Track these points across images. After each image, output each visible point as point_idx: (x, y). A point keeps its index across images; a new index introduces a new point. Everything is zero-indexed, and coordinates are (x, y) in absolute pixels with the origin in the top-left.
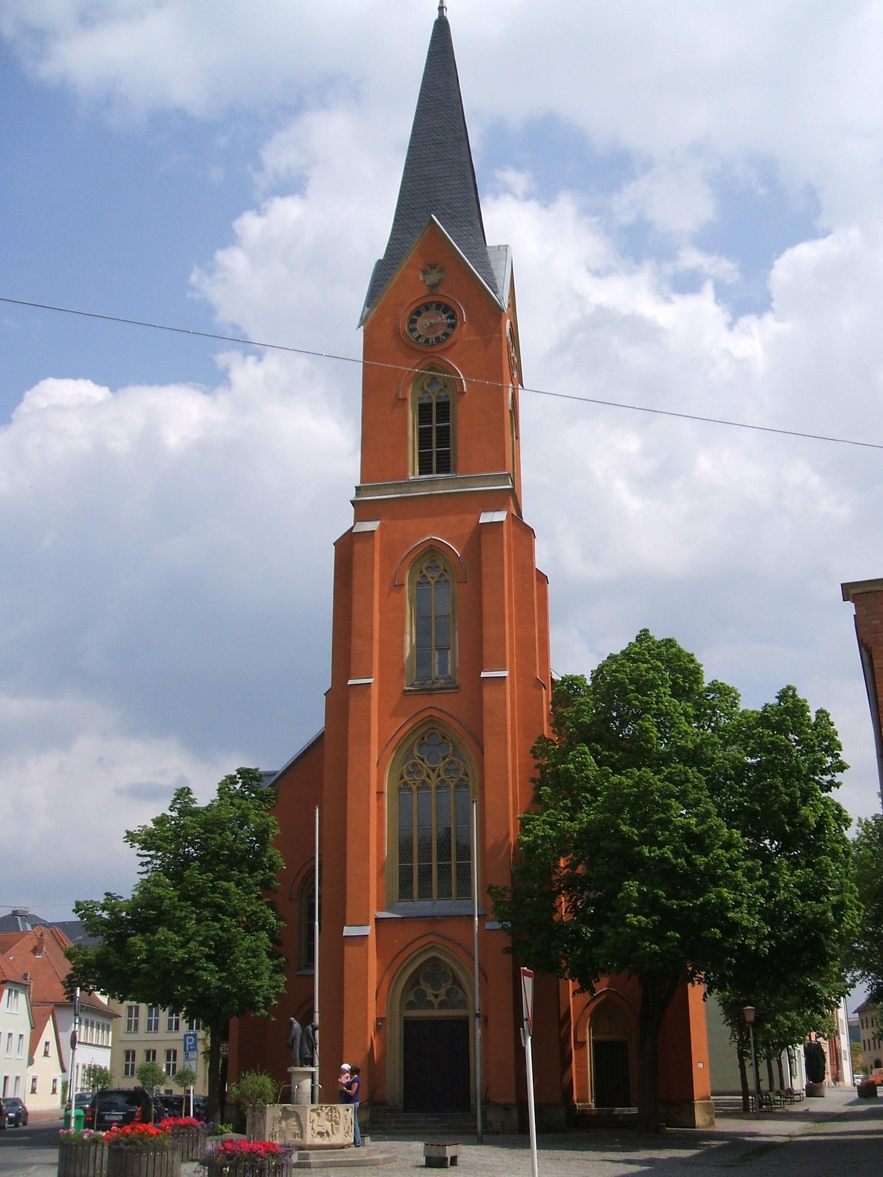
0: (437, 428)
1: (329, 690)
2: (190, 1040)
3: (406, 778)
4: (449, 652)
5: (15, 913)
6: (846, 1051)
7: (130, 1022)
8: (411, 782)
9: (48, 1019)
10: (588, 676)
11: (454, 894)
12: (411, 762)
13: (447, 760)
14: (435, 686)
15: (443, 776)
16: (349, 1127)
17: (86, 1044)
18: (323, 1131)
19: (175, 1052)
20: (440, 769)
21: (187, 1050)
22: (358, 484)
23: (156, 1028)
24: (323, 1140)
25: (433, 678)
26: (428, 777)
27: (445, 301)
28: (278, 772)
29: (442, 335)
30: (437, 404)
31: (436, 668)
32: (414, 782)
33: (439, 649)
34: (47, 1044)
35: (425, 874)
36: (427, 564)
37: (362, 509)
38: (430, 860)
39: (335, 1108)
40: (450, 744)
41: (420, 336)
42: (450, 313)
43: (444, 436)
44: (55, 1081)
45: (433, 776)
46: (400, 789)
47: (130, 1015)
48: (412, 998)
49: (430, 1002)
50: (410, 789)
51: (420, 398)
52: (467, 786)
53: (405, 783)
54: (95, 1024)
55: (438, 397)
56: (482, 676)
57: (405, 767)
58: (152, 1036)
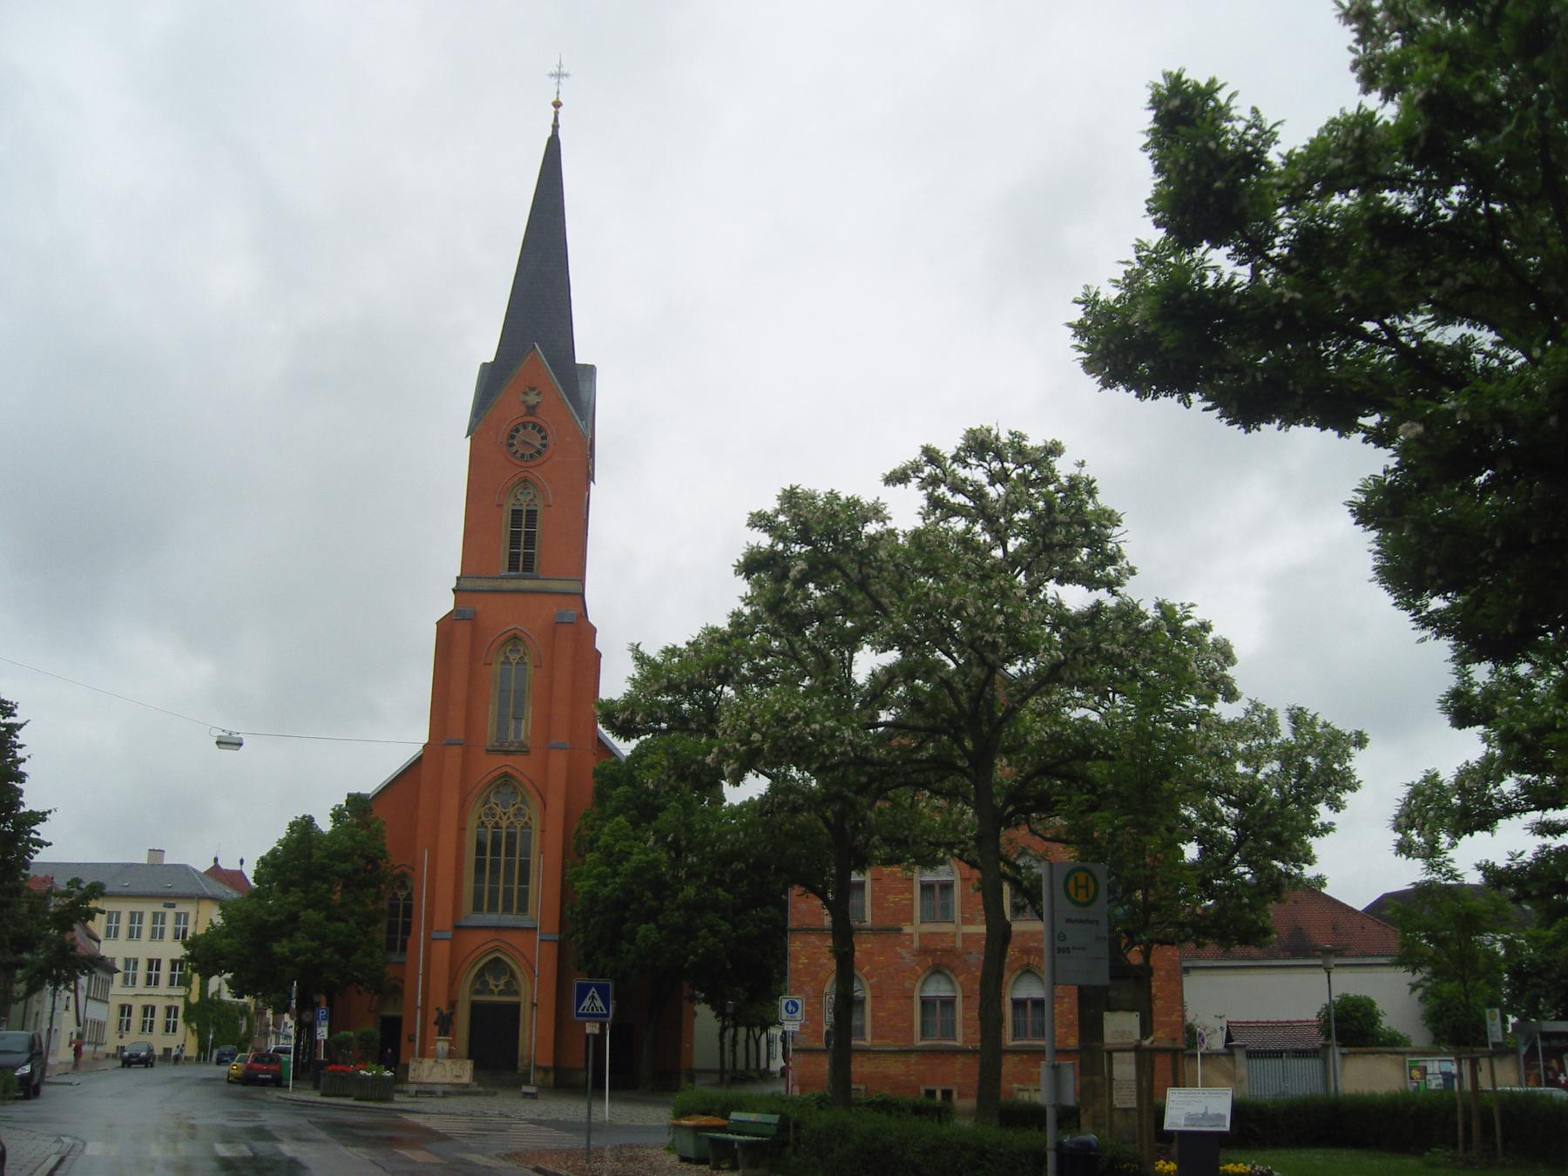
14: (512, 748)
19: (153, 1008)
27: (539, 422)
38: (504, 889)
42: (543, 434)
43: (530, 540)
45: (505, 818)
48: (478, 986)
52: (530, 828)
53: (483, 823)
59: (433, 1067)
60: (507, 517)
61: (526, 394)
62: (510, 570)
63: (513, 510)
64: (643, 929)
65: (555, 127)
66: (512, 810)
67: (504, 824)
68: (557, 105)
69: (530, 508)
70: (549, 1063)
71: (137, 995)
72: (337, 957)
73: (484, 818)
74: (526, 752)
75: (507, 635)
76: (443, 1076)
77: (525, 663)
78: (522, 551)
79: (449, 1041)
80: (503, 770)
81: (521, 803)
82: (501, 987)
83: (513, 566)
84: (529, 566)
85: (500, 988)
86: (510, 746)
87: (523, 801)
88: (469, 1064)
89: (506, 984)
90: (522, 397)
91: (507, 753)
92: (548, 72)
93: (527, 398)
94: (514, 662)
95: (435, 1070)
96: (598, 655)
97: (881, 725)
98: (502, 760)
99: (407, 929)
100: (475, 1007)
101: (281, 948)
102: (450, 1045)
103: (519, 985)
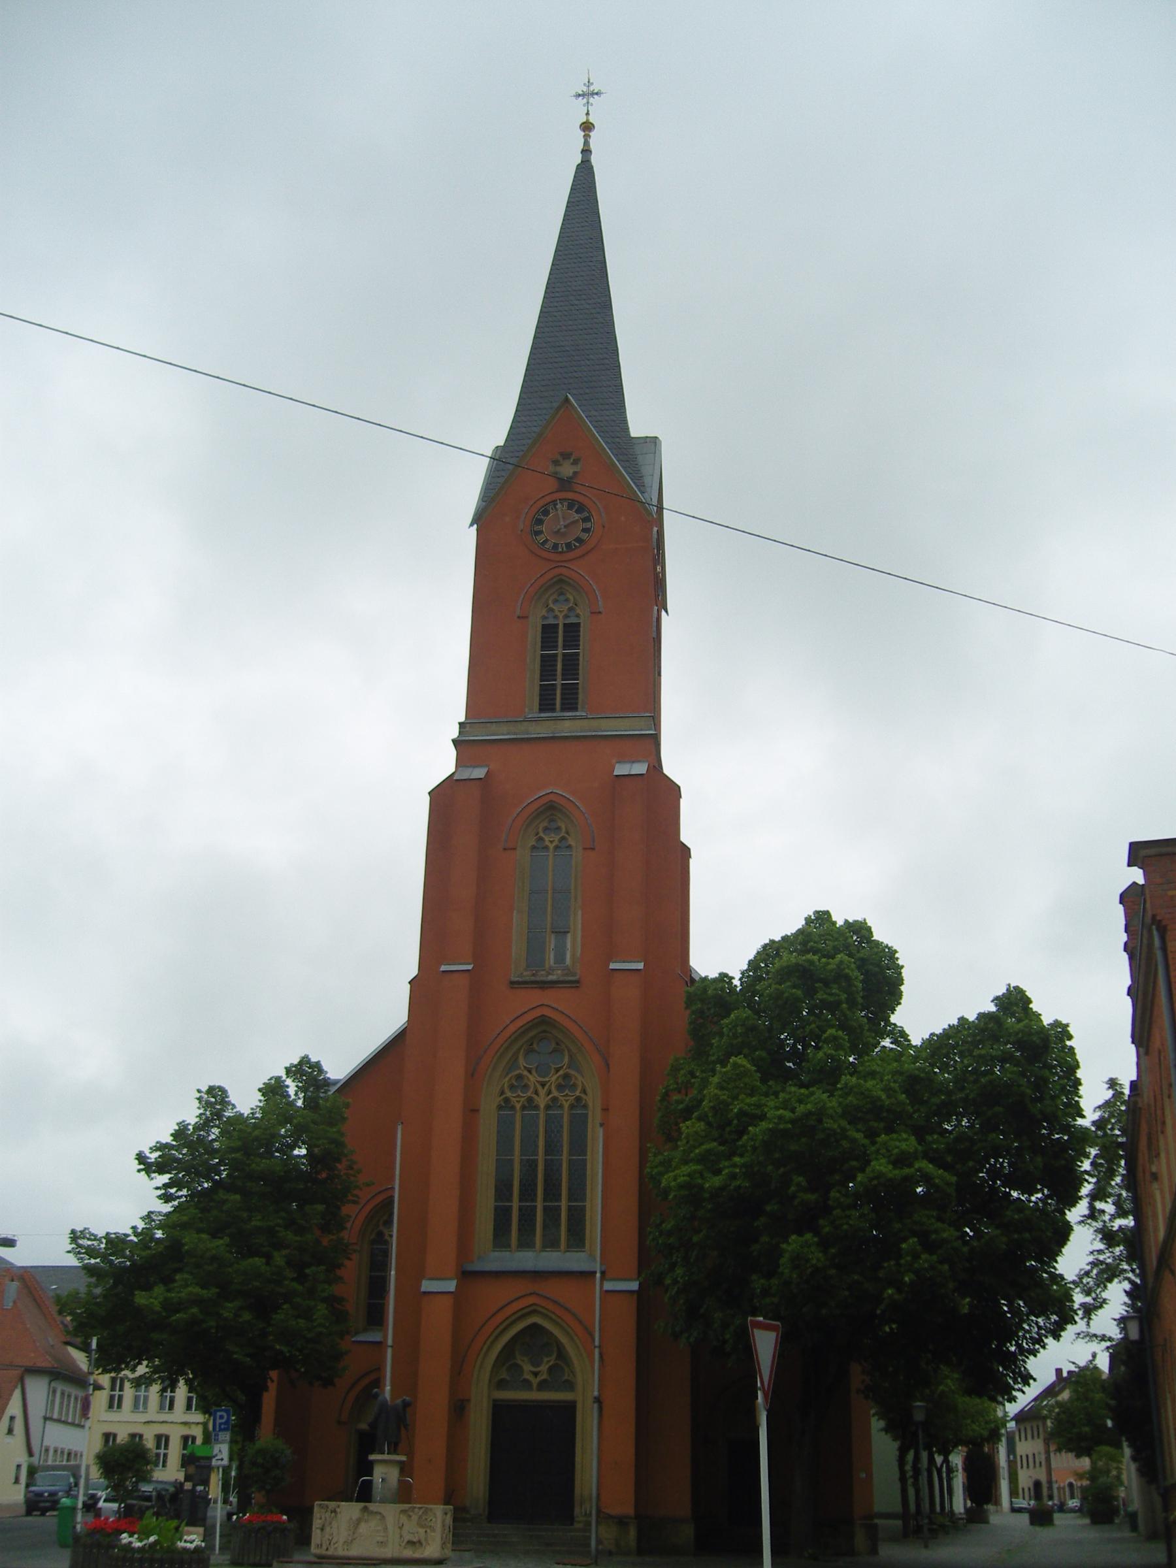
0: (564, 655)
1: (415, 978)
2: (221, 1417)
4: (569, 935)
5: (149, 1213)
6: (1004, 1468)
7: (112, 1398)
8: (514, 1099)
9: (16, 1387)
10: (737, 975)
13: (561, 1072)
14: (550, 978)
15: (555, 1093)
16: (446, 1536)
17: (59, 1421)
18: (415, 1540)
19: (167, 1438)
20: (551, 1084)
21: (218, 1430)
22: (463, 719)
23: (119, 1406)
24: (414, 1553)
25: (547, 966)
26: (536, 1093)
27: (581, 499)
28: (340, 1080)
29: (574, 540)
31: (552, 956)
32: (518, 1099)
33: (556, 932)
34: (12, 1418)
35: (527, 1218)
36: (545, 824)
39: (431, 1509)
40: (566, 1053)
41: (546, 541)
43: (571, 666)
44: (19, 1466)
45: (542, 1092)
47: (113, 1389)
49: (526, 1381)
50: (513, 1108)
51: (544, 618)
52: (585, 1106)
53: (507, 1100)
54: (66, 1394)
56: (610, 967)
57: (507, 1079)
58: (113, 1416)
59: (359, 1521)
60: (534, 635)
61: (556, 463)
62: (541, 710)
63: (543, 625)
64: (793, 1244)
65: (586, 151)
66: (553, 1079)
67: (542, 1101)
68: (587, 127)
69: (568, 621)
70: (627, 1509)
71: (148, 1422)
72: (247, 1316)
73: (508, 1094)
74: (576, 984)
75: (542, 801)
76: (382, 1544)
77: (569, 847)
78: (560, 651)
79: (401, 1463)
80: (538, 1013)
82: (544, 1376)
83: (546, 704)
84: (570, 703)
85: (539, 1378)
86: (549, 974)
87: (572, 1063)
88: (440, 1515)
89: (550, 1369)
91: (544, 985)
93: (558, 469)
94: (551, 846)
95: (363, 1528)
96: (685, 852)
98: (535, 997)
100: (500, 1410)
101: (149, 1299)
103: (573, 1373)
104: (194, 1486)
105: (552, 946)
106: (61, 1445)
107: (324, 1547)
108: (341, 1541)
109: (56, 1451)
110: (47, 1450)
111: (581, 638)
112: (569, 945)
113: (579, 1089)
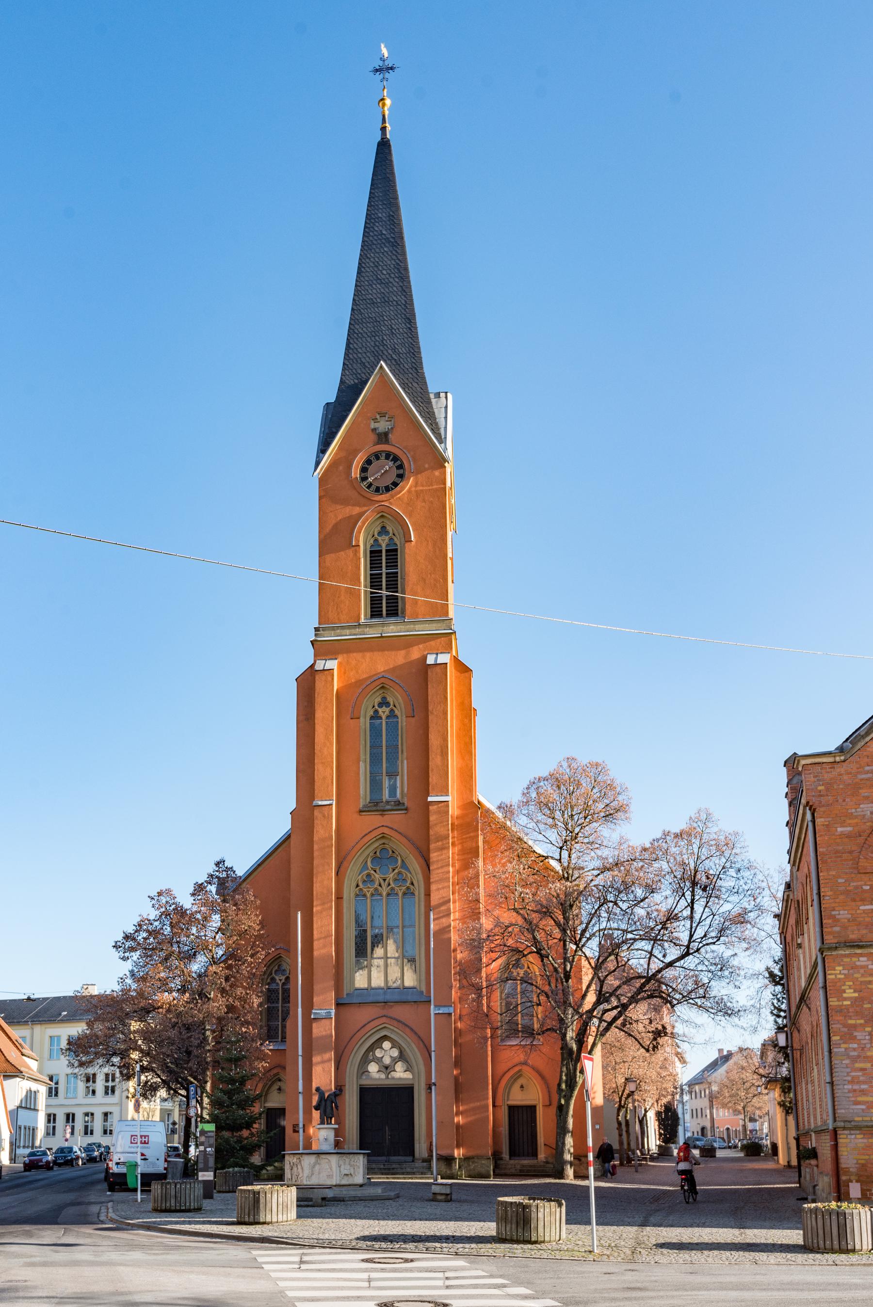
3: (361, 886)
11: (384, 612)
12: (366, 872)
13: (396, 871)
17: (26, 1108)
23: (56, 1095)
26: (380, 885)
30: (387, 551)
37: (321, 649)
43: (393, 583)
45: (384, 885)
46: (357, 895)
50: (365, 896)
55: (387, 545)
57: (360, 877)
81: (402, 867)
83: (375, 612)
88: (360, 1162)
90: (373, 425)
92: (372, 69)
93: (377, 425)
97: (846, 999)
99: (287, 999)
102: (336, 1135)
104: (205, 1148)
105: (387, 785)
106: (27, 1125)
107: (294, 1180)
108: (305, 1175)
109: (25, 1128)
110: (20, 1128)
111: (399, 560)
112: (398, 784)
113: (409, 882)
